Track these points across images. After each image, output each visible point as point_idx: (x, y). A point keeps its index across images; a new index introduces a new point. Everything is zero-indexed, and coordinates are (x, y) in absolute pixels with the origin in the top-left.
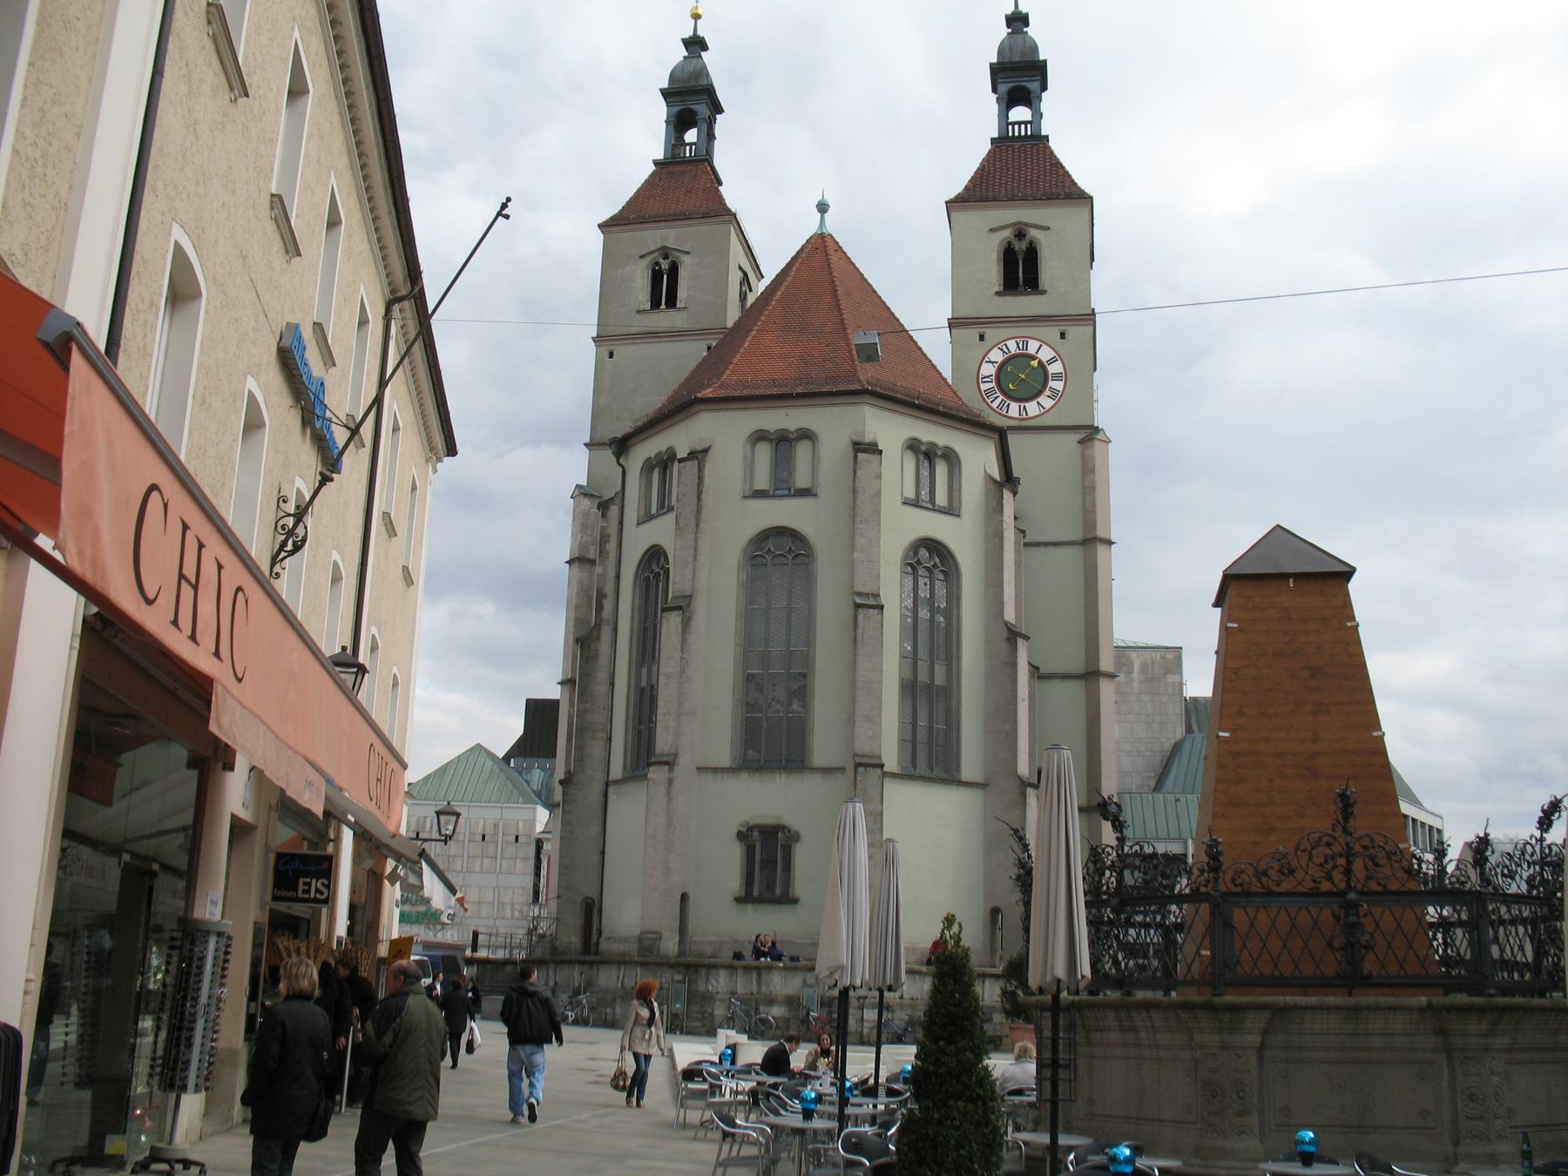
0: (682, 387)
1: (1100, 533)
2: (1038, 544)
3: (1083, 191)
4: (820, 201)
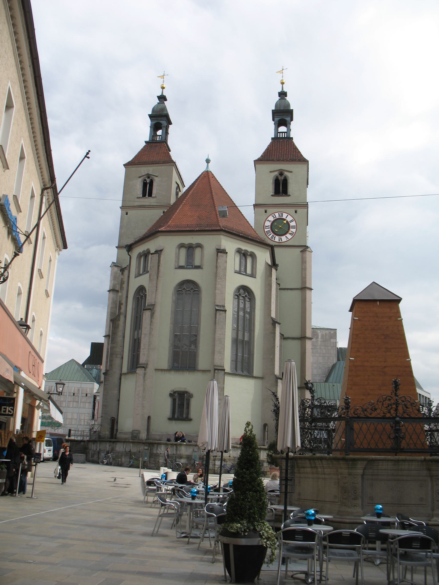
0: (153, 226)
1: (308, 286)
2: (284, 289)
3: (305, 158)
4: (207, 159)
